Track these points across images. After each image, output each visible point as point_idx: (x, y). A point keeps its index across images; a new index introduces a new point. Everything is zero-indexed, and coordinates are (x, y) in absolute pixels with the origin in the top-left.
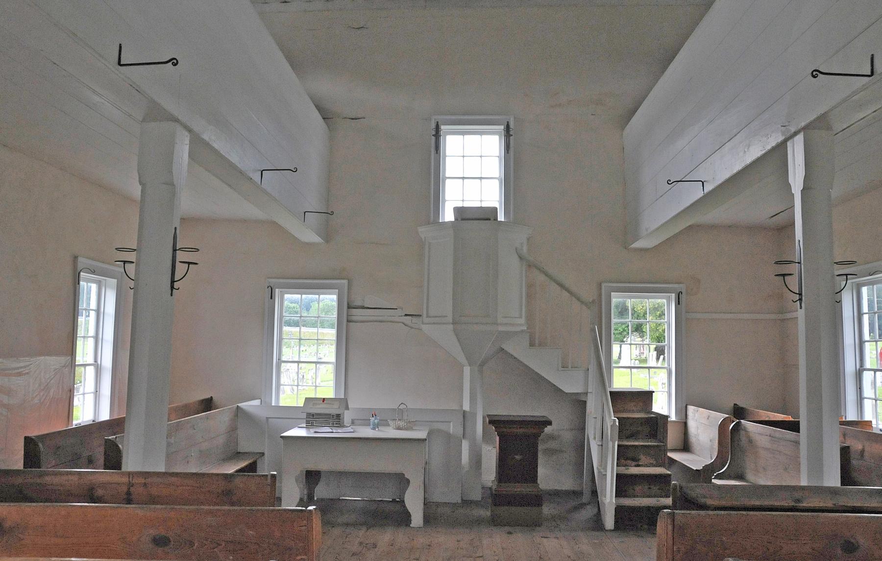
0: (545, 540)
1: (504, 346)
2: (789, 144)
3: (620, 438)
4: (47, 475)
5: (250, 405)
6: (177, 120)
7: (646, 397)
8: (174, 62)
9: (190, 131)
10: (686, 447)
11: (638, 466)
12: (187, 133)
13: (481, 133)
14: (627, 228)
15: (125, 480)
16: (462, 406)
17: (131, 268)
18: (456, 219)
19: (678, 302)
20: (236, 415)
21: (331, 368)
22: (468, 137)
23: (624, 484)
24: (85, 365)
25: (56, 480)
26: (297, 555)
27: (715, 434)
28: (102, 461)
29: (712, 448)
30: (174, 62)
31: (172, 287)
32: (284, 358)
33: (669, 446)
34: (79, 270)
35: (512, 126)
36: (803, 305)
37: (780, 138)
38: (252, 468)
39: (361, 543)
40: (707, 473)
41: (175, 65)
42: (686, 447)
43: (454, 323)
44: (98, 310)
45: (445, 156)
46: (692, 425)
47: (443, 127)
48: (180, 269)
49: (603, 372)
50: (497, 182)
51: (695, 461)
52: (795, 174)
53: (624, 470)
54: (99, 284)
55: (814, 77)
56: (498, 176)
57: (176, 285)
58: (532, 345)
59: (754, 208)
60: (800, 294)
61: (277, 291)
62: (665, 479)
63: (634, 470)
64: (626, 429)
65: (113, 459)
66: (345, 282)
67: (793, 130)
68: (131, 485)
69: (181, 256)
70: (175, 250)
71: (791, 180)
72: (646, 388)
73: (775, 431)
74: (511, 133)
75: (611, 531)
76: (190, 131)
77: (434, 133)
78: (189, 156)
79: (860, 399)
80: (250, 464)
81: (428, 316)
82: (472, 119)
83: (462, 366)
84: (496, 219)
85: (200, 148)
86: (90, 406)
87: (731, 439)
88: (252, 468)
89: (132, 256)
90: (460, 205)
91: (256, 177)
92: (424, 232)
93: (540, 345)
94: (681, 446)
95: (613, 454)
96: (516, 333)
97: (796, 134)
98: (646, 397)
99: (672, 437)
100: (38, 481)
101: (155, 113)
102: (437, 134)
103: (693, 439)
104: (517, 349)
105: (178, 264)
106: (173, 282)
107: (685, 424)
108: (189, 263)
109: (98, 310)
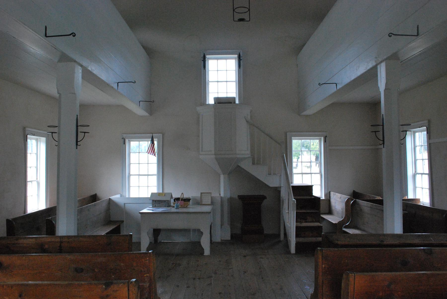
0: (261, 259)
1: (239, 165)
2: (378, 67)
3: (297, 209)
4: (21, 239)
5: (116, 197)
6: (75, 61)
7: (309, 189)
8: (74, 35)
9: (81, 66)
10: (330, 212)
11: (306, 222)
12: (80, 68)
13: (226, 59)
14: (299, 106)
15: (58, 240)
16: (220, 194)
17: (55, 136)
18: (215, 103)
19: (325, 141)
20: (121, 221)
21: (155, 178)
22: (220, 61)
23: (299, 231)
24: (31, 181)
25: (25, 241)
26: (144, 274)
27: (344, 205)
28: (44, 229)
29: (342, 212)
30: (74, 35)
31: (77, 145)
32: (131, 173)
33: (322, 212)
34: (26, 133)
35: (241, 55)
36: (385, 146)
37: (374, 64)
38: (117, 231)
39: (173, 264)
40: (341, 224)
41: (74, 36)
42: (330, 212)
43: (215, 154)
44: (37, 152)
45: (208, 71)
46: (333, 201)
47: (207, 56)
48: (81, 136)
49: (288, 177)
50: (235, 83)
51: (334, 219)
52: (381, 82)
53: (299, 225)
54: (37, 140)
55: (390, 36)
56: (235, 80)
57: (79, 143)
58: (253, 164)
59: (362, 94)
60: (383, 141)
61: (127, 141)
62: (320, 228)
63: (304, 224)
64: (300, 204)
65: (51, 229)
66: (161, 135)
67: (380, 60)
68: (61, 242)
69: (80, 129)
70: (77, 126)
71: (379, 85)
72: (309, 184)
73: (372, 205)
74: (241, 58)
75: (293, 254)
76: (81, 66)
77: (203, 59)
78: (82, 78)
79: (415, 188)
80: (116, 228)
81: (202, 151)
82: (222, 51)
83: (219, 175)
84: (235, 103)
85: (88, 76)
86: (36, 200)
87: (352, 209)
88: (117, 231)
89: (56, 130)
90: (216, 96)
91: (115, 86)
92: (199, 109)
93: (257, 164)
94: (327, 212)
95: (294, 217)
96: (246, 158)
97: (381, 62)
98: (309, 189)
99: (323, 207)
100: (16, 242)
101: (64, 58)
102: (204, 60)
103: (333, 208)
104: (247, 166)
105: (79, 133)
106: (77, 142)
107: (329, 201)
108: (85, 133)
109: (37, 152)
